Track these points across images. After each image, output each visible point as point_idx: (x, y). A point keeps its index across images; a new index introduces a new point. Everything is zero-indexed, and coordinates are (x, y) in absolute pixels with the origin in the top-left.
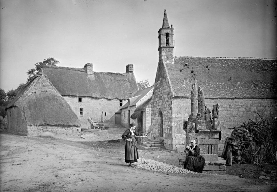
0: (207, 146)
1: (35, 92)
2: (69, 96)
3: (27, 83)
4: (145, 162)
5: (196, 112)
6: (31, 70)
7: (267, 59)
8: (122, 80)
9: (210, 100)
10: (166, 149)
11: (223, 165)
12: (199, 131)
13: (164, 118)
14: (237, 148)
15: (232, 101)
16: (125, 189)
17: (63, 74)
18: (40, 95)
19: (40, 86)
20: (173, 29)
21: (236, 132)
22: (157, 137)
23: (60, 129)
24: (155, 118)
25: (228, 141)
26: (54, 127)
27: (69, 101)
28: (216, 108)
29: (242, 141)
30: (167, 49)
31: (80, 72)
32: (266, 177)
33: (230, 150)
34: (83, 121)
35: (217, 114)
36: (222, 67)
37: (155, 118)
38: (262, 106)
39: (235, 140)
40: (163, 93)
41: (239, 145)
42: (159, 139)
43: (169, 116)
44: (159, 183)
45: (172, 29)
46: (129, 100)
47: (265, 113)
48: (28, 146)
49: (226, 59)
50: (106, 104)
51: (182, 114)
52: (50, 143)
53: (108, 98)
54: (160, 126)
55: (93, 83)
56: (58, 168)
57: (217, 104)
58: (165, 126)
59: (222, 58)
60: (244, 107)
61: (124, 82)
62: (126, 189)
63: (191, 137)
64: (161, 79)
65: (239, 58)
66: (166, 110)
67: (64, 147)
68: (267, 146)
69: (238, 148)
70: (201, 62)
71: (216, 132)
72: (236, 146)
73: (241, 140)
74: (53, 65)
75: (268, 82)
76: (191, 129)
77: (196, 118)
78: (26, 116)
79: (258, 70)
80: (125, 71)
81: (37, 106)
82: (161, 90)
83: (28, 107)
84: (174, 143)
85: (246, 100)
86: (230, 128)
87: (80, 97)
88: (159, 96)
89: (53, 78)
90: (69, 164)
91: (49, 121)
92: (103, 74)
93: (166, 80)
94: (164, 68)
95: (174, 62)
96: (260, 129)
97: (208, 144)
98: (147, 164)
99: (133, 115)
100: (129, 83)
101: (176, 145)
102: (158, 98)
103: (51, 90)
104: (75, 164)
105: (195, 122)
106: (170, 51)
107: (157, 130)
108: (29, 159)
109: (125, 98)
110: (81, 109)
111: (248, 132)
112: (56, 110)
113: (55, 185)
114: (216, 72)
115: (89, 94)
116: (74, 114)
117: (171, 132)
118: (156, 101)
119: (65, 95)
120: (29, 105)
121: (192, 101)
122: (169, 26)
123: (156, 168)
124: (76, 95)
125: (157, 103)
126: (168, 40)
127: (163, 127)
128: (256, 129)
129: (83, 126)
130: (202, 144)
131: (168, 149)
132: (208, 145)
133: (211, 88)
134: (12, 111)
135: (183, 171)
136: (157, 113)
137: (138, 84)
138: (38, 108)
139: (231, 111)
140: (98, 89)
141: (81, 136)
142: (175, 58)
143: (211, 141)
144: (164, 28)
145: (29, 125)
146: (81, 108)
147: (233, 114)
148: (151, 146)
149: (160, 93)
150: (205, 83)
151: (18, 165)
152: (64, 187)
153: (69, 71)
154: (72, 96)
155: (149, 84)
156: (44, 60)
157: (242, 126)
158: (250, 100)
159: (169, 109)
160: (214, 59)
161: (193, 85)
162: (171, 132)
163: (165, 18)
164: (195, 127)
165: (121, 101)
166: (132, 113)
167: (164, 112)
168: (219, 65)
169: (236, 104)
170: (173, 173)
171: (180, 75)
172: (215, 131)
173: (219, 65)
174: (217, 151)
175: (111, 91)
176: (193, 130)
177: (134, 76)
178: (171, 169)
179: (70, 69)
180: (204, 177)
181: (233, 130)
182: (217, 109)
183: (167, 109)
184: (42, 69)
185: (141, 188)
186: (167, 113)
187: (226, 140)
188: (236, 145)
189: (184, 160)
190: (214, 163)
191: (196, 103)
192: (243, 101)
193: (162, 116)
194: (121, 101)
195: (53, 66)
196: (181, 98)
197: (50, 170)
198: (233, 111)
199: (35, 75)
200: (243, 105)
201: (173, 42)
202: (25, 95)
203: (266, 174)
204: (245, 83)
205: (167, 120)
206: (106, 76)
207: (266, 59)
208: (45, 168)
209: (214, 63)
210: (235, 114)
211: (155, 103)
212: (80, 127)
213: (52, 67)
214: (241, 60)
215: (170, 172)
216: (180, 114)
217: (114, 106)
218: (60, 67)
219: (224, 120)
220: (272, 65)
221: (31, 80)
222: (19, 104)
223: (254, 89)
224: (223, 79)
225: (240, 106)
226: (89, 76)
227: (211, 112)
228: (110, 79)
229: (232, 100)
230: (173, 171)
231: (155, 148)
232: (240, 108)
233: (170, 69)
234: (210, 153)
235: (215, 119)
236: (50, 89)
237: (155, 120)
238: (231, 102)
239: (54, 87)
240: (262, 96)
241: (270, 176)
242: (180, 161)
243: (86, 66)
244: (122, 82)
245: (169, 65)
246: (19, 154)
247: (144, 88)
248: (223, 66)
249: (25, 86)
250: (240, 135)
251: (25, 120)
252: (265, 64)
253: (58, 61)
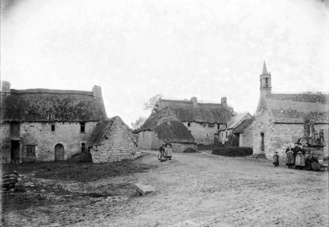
45: (270, 75)
149: (262, 120)
159: (271, 131)
167: (265, 134)
190: (261, 163)
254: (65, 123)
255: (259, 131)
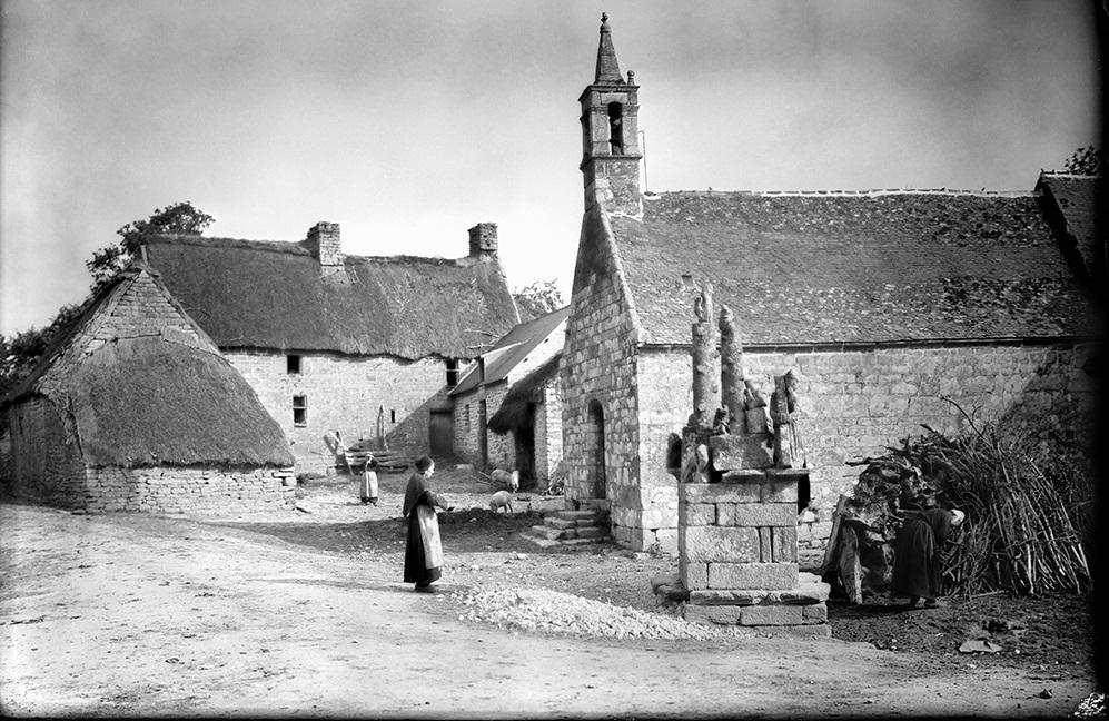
0: (756, 530)
1: (116, 340)
2: (251, 349)
3: (85, 303)
4: (519, 600)
5: (713, 402)
6: (103, 253)
7: (997, 196)
8: (456, 284)
9: (781, 354)
10: (619, 548)
11: (817, 602)
12: (725, 475)
13: (608, 429)
14: (878, 537)
15: (866, 358)
16: (423, 703)
17: (227, 266)
18: (135, 349)
19: (136, 313)
20: (638, 87)
21: (873, 478)
22: (585, 501)
23: (214, 477)
24: (576, 429)
25: (842, 509)
26: (188, 471)
27: (250, 371)
28: (787, 387)
29: (898, 510)
30: (616, 165)
31: (290, 258)
32: (986, 645)
33: (854, 546)
34: (307, 449)
35: (791, 409)
36: (826, 230)
37: (576, 429)
38: (983, 373)
39: (868, 506)
40: (604, 331)
41: (888, 527)
42: (593, 509)
43: (627, 420)
44: (560, 677)
45: (632, 90)
46: (481, 361)
47: (993, 398)
48: (82, 550)
49: (840, 197)
50: (393, 377)
51: (676, 410)
52: (170, 532)
53: (403, 355)
54: (593, 459)
55: (343, 299)
56: (184, 630)
57: (789, 373)
58: (614, 457)
59: (825, 193)
60: (912, 378)
61: (464, 293)
62: (427, 703)
63: (693, 501)
64: (593, 278)
65: (890, 193)
66: (617, 397)
67: (221, 546)
68: (991, 525)
69: (884, 536)
70: (745, 209)
71: (788, 480)
72: (873, 529)
73: (892, 507)
74: (189, 231)
75: (1001, 282)
76: (694, 469)
77: (711, 425)
78: (82, 430)
79: (963, 237)
80: (465, 250)
81: (123, 395)
82: (594, 322)
83: (88, 399)
84: (647, 523)
85: (920, 354)
86: (854, 461)
87: (295, 354)
88: (587, 343)
89: (187, 284)
90: (229, 614)
91: (172, 448)
92: (381, 264)
93: (612, 284)
94: (607, 235)
95: (642, 215)
96: (964, 461)
97: (760, 524)
98: (528, 606)
99: (500, 415)
100: (480, 295)
101: (653, 530)
102: (586, 352)
103: (176, 328)
104: (254, 611)
105: (707, 443)
106: (625, 173)
107: (583, 476)
108: (77, 598)
109: (469, 352)
110: (299, 400)
111: (919, 474)
112: (198, 406)
113: (161, 696)
114: (802, 246)
115: (327, 339)
116: (270, 420)
117: (635, 479)
118: (580, 364)
119: (234, 349)
120: (93, 390)
121: (697, 361)
122: (619, 75)
123: (558, 622)
124: (278, 347)
125: (581, 371)
126: (617, 132)
127: (607, 463)
128: (950, 464)
129: (305, 464)
130: (736, 525)
131: (625, 548)
132: (759, 528)
133: (787, 310)
134: (29, 415)
135: (662, 631)
136: (584, 408)
137: (518, 297)
138: (126, 400)
139: (862, 394)
140: (361, 320)
141: (299, 504)
142: (647, 197)
143: (768, 513)
144: (600, 84)
145: (91, 467)
146: (299, 395)
147: (872, 407)
148: (562, 537)
149: (591, 332)
150: (760, 292)
151: (32, 621)
152: (193, 701)
153: (247, 252)
154: (262, 350)
155: (558, 296)
156: (156, 214)
157: (896, 452)
158: (936, 353)
159: (626, 391)
160: (793, 197)
161: (700, 301)
162: (635, 479)
163: (604, 45)
164: (706, 459)
165: (451, 364)
166: (493, 410)
168: (814, 222)
169: (880, 371)
170: (620, 636)
171: (667, 263)
172: (785, 472)
173: (814, 222)
174: (794, 550)
175: (413, 327)
176: (702, 471)
177: (499, 269)
178: (615, 625)
179: (254, 246)
180: (738, 652)
181: (865, 467)
182: (790, 389)
183: (619, 392)
184: (143, 247)
185: (488, 698)
186: (620, 409)
187: (837, 507)
188: (875, 525)
189: (669, 588)
190: (782, 597)
191: (712, 369)
192: (909, 354)
193: (603, 420)
194: (451, 364)
195: (188, 237)
196: (669, 351)
197: (151, 640)
198: (870, 396)
199: (120, 271)
200: (907, 371)
201: (636, 139)
202: (76, 353)
203: (986, 634)
204: (914, 289)
205: (620, 434)
206: (390, 271)
207: (993, 195)
208: (135, 632)
209: (795, 213)
210: (877, 407)
211: (576, 370)
212: (292, 469)
213: (181, 241)
214: (901, 198)
215: (611, 635)
216: (669, 410)
217: (427, 380)
218: (212, 239)
219: (835, 430)
220: (1017, 218)
221: (103, 292)
222: (54, 385)
223: (950, 311)
224: (830, 274)
225: (898, 377)
226: (326, 272)
227: (768, 400)
228: (408, 283)
229: (867, 353)
230: (622, 630)
231: (578, 544)
232: (895, 382)
233: (626, 239)
234: (767, 555)
235: (784, 429)
236: (172, 327)
237: (577, 435)
238: (862, 360)
239: (190, 316)
240: (982, 334)
241: (1003, 642)
242: (656, 590)
243: (314, 234)
244: (455, 291)
245: (623, 225)
246: (43, 581)
247: (539, 314)
248: (832, 222)
249: (77, 314)
250: (889, 486)
251: (76, 446)
252: (991, 212)
253: (209, 217)
254: (431, 563)
255: (583, 392)
